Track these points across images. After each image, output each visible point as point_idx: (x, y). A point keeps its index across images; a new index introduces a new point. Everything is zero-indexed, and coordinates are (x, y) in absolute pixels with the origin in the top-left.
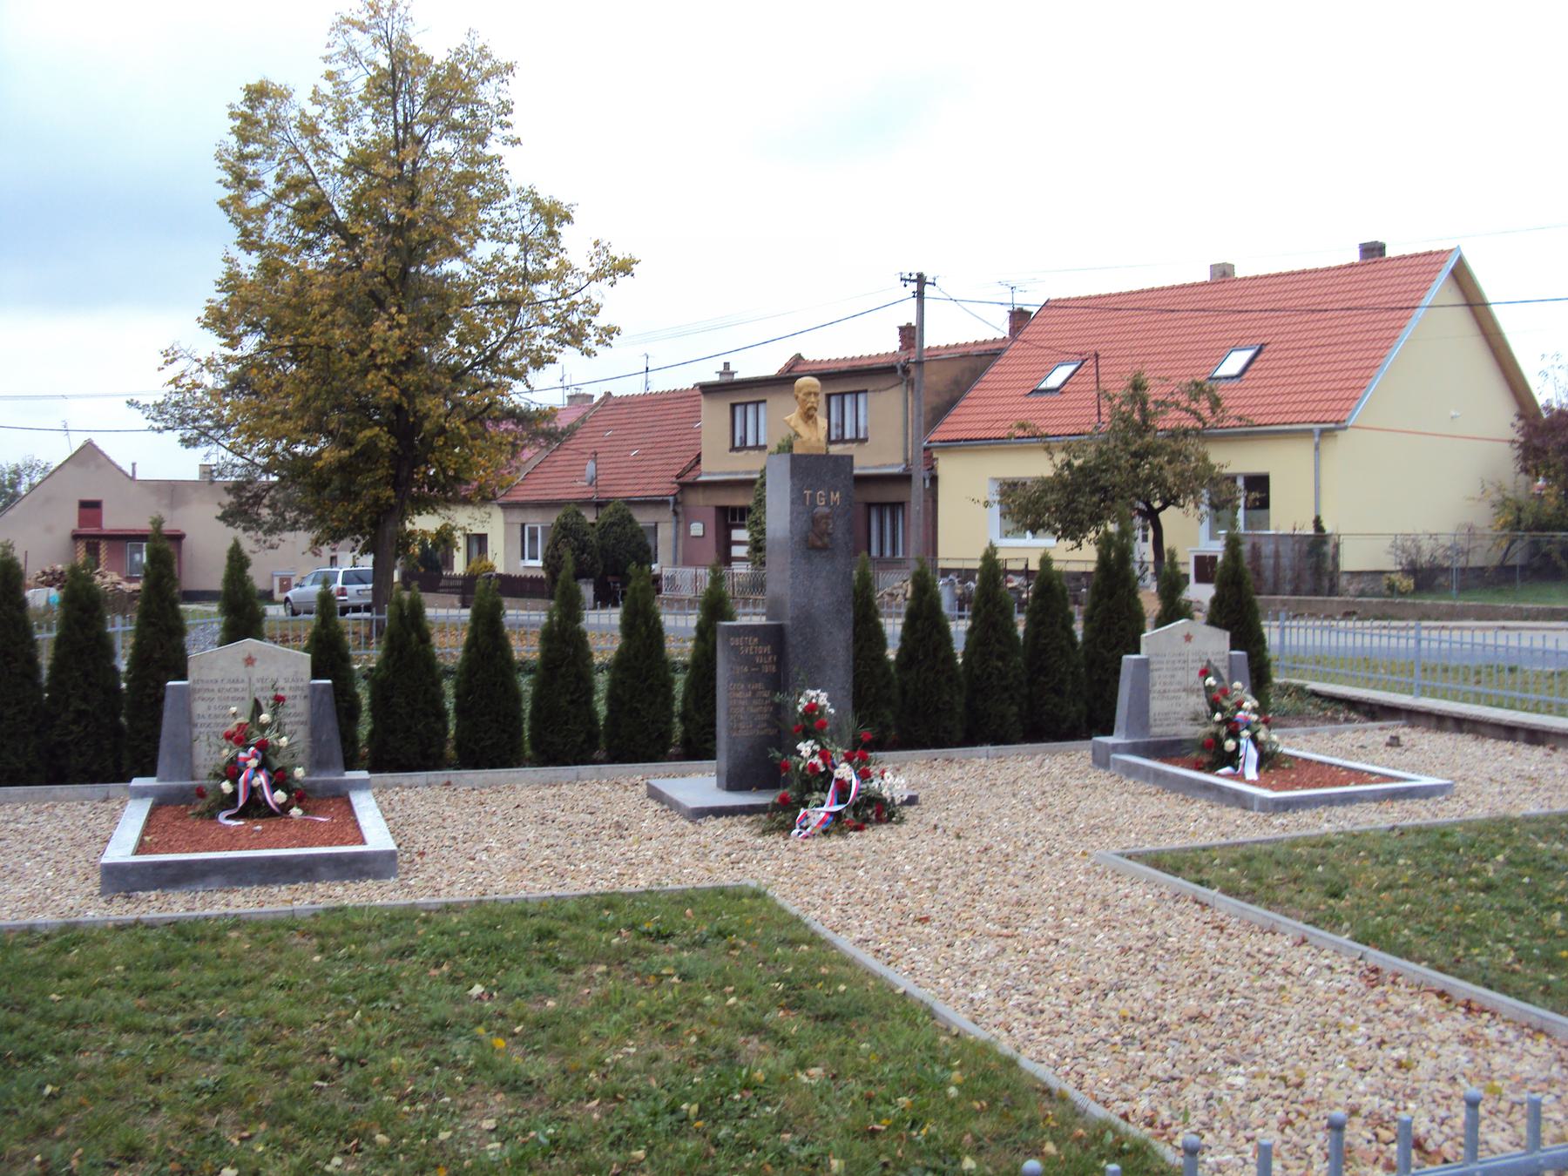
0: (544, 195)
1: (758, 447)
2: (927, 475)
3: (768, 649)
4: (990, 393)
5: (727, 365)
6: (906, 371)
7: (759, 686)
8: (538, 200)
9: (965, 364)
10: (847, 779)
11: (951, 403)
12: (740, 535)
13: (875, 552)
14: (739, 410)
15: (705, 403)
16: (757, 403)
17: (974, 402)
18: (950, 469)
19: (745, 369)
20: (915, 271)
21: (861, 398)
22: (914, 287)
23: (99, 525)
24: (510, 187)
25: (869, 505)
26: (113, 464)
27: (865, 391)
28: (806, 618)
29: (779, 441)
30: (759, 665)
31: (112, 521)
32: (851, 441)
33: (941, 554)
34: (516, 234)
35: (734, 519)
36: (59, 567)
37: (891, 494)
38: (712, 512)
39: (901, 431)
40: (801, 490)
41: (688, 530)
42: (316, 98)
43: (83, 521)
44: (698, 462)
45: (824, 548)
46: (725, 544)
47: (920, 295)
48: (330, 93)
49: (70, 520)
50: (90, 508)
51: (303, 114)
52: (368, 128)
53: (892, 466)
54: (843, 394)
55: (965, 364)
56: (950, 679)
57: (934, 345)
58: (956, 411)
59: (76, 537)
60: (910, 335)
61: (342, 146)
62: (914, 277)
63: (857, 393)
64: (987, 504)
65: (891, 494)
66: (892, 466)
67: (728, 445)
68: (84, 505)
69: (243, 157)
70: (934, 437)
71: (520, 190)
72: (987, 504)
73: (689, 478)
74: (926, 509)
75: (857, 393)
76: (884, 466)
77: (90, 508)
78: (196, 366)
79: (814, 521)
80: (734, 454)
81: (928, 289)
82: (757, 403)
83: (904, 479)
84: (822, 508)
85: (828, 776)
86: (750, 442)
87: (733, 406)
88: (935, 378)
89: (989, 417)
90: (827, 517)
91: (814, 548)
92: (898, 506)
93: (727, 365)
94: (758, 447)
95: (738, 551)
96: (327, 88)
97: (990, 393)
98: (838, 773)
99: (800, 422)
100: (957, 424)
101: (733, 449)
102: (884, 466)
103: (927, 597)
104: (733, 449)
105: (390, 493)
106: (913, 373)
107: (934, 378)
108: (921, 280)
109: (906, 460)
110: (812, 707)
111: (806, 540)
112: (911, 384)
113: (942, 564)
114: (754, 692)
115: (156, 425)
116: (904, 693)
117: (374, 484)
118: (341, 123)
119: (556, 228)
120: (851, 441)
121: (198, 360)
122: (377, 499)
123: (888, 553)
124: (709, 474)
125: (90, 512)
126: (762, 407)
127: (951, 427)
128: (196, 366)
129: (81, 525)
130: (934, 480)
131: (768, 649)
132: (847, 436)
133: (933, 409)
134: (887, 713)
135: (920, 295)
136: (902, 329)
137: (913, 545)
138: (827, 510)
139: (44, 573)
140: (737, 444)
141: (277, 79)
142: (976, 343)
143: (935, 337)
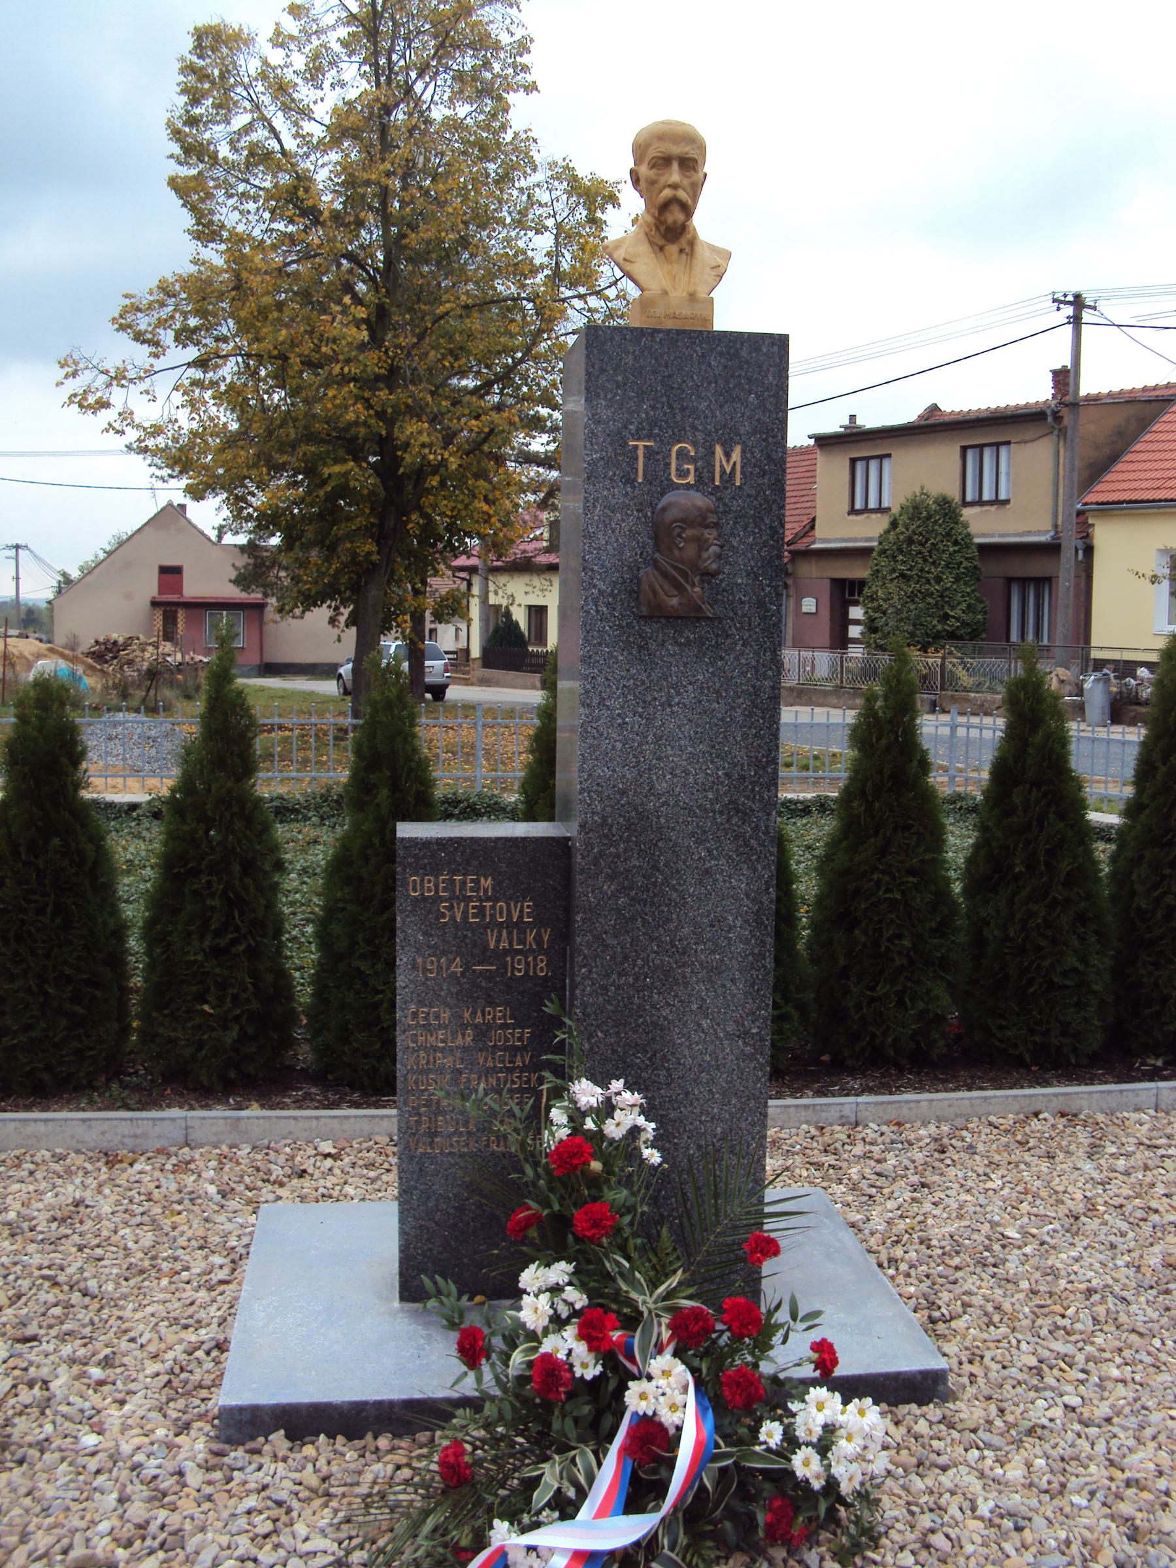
0: (583, 172)
1: (881, 510)
2: (1080, 544)
3: (524, 910)
4: (1160, 446)
5: (853, 417)
6: (1057, 418)
7: (498, 1014)
8: (575, 178)
9: (1130, 410)
10: (668, 1418)
11: (1114, 458)
12: (856, 612)
13: (1014, 637)
14: (860, 467)
15: (820, 457)
16: (881, 458)
17: (1140, 457)
18: (1111, 540)
19: (869, 421)
20: (1072, 288)
21: (1003, 451)
22: (1069, 311)
23: (180, 592)
24: (537, 158)
25: (1009, 580)
26: (195, 527)
27: (1008, 443)
28: (631, 828)
29: (902, 501)
30: (499, 956)
31: (194, 588)
32: (990, 503)
33: (1094, 642)
34: (550, 223)
35: (852, 594)
36: (115, 636)
37: (1036, 567)
38: (826, 586)
39: (1050, 489)
40: (619, 440)
41: (799, 605)
42: (279, 40)
43: (162, 588)
44: (813, 527)
45: (692, 616)
46: (841, 622)
47: (1076, 321)
48: (296, 33)
49: (150, 587)
50: (170, 574)
51: (265, 62)
52: (352, 81)
53: (1039, 533)
54: (981, 447)
55: (1130, 410)
56: (1081, 918)
57: (1094, 391)
58: (1119, 467)
59: (155, 604)
60: (1064, 379)
61: (324, 103)
62: (1070, 298)
63: (997, 445)
64: (1154, 579)
65: (1036, 567)
66: (1039, 533)
67: (846, 507)
68: (164, 570)
69: (193, 121)
70: (1090, 498)
71: (552, 165)
72: (1154, 579)
73: (801, 546)
74: (1077, 585)
75: (997, 445)
76: (1029, 533)
77: (170, 574)
78: (103, 378)
79: (661, 533)
80: (854, 517)
81: (1087, 316)
82: (881, 458)
83: (1051, 549)
84: (686, 499)
85: (605, 1396)
86: (872, 504)
87: (853, 461)
88: (1089, 427)
89: (1159, 475)
90: (700, 520)
91: (657, 614)
92: (1044, 582)
93: (853, 417)
94: (881, 510)
95: (854, 631)
96: (291, 26)
97: (1160, 446)
98: (638, 1399)
99: (644, 248)
100: (1118, 483)
101: (853, 511)
102: (1029, 533)
103: (1038, 738)
104: (853, 511)
105: (370, 546)
106: (1067, 421)
107: (1092, 428)
108: (1078, 302)
109: (1056, 526)
110: (585, 1141)
111: (632, 590)
112: (1063, 433)
113: (1095, 654)
114: (482, 1033)
115: (159, 473)
116: (979, 942)
117: (351, 536)
118: (314, 74)
119: (599, 214)
120: (990, 503)
121: (106, 372)
122: (355, 555)
123: (1030, 637)
124: (824, 541)
125: (169, 577)
126: (886, 463)
127: (1108, 489)
128: (103, 378)
129: (160, 592)
130: (1089, 550)
131: (524, 910)
132: (986, 497)
133: (1091, 465)
134: (939, 990)
135: (1076, 321)
136: (1055, 373)
137: (1059, 630)
138: (700, 500)
139: (97, 642)
140: (859, 505)
141: (233, 18)
142: (1145, 389)
143: (1090, 384)
